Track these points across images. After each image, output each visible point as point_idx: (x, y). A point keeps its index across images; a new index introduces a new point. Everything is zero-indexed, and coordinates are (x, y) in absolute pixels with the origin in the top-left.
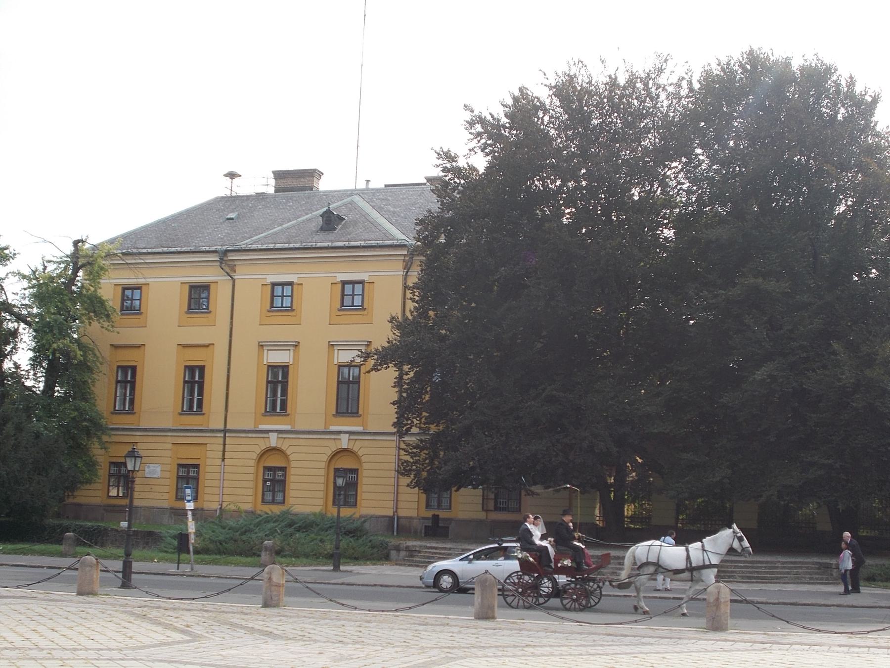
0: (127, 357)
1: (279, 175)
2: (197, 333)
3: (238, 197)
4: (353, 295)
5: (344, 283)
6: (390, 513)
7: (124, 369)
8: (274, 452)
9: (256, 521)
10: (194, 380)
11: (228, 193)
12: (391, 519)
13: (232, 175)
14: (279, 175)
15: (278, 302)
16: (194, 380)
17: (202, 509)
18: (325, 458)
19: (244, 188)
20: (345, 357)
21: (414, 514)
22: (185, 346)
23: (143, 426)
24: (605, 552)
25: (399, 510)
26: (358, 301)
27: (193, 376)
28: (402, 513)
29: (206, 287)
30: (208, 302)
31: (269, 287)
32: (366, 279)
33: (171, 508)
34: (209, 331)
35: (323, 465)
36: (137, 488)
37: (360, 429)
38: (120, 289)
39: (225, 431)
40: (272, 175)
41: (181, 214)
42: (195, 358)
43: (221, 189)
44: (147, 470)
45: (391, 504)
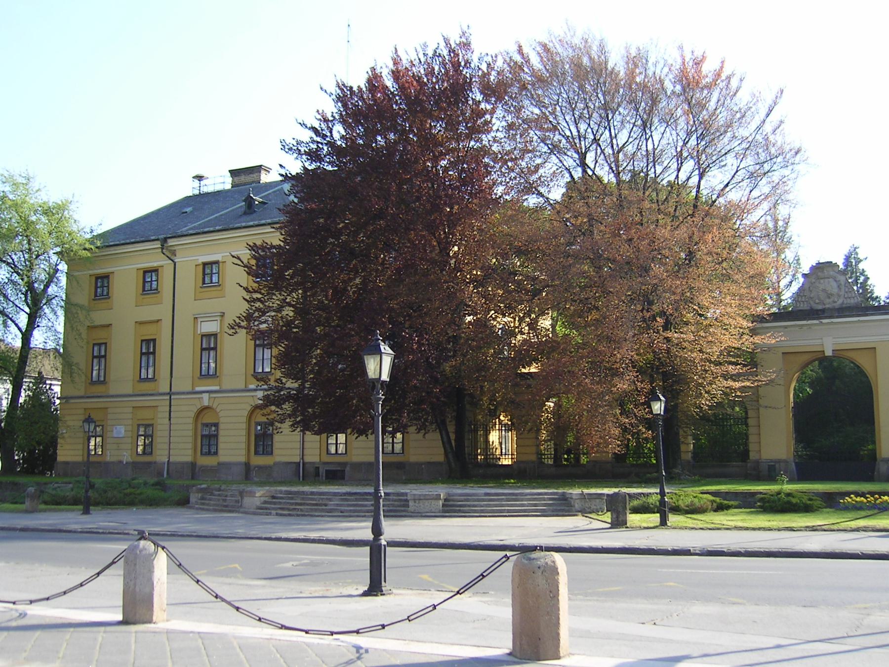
0: (100, 336)
1: (234, 173)
2: (148, 312)
3: (208, 194)
4: (212, 274)
5: (205, 264)
6: (297, 459)
7: (148, 341)
8: (206, 411)
9: (193, 470)
10: (148, 349)
11: (197, 192)
12: (192, 463)
13: (200, 178)
14: (234, 173)
15: (148, 286)
16: (148, 349)
17: (155, 463)
18: (192, 415)
19: (209, 187)
20: (210, 327)
21: (316, 459)
22: (141, 323)
23: (112, 392)
24: (616, 490)
25: (305, 457)
26: (215, 279)
27: (148, 348)
28: (308, 459)
29: (155, 270)
30: (144, 286)
31: (201, 267)
32: (220, 259)
33: (133, 463)
34: (159, 310)
35: (191, 420)
36: (59, 447)
37: (217, 388)
38: (93, 279)
39: (170, 394)
40: (229, 174)
41: (153, 213)
42: (148, 332)
43: (189, 189)
44: (115, 431)
45: (298, 452)
